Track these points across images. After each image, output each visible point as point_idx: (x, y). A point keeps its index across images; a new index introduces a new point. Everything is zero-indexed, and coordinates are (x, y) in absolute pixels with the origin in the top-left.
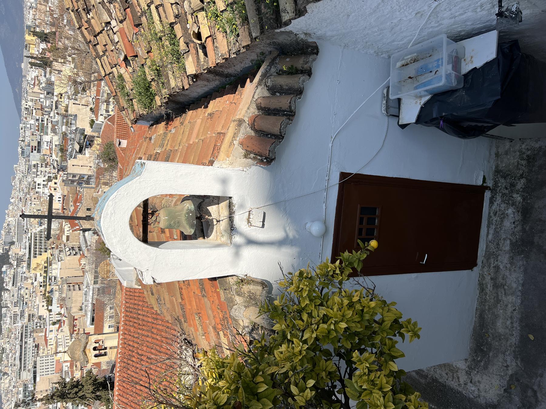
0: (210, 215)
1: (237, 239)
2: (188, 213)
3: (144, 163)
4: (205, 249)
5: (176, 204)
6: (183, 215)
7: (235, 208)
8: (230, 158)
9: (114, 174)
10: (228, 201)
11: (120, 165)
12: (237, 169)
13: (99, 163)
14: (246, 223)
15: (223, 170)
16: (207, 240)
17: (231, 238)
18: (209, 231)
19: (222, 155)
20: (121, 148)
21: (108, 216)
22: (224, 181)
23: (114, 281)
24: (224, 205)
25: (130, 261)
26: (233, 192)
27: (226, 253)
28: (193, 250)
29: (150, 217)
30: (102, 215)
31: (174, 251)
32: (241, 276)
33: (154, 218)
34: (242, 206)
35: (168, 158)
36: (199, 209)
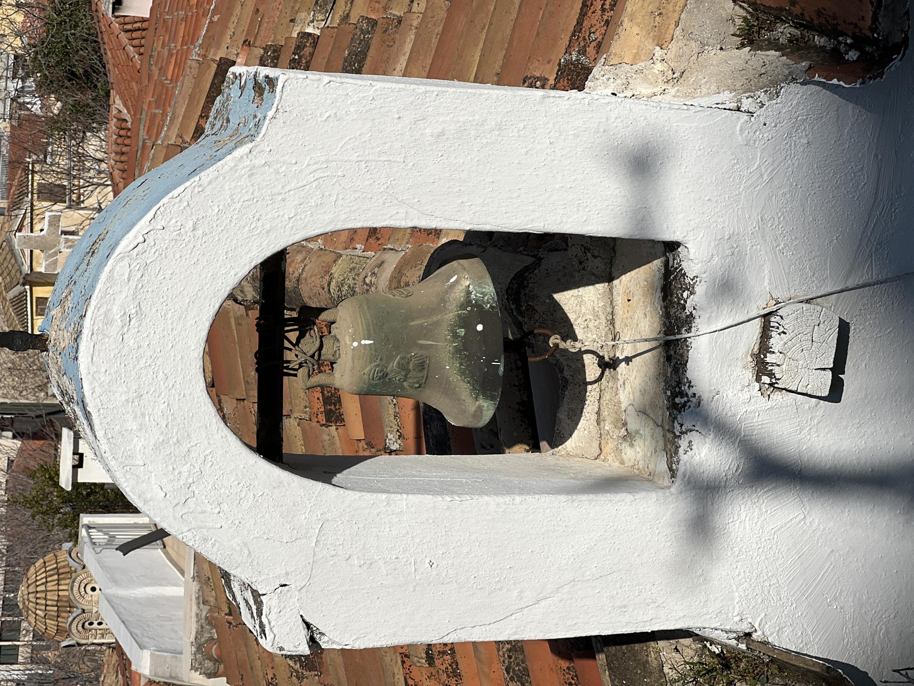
0: (569, 333)
1: (704, 454)
2: (466, 322)
3: (271, 82)
4: (546, 500)
5: (397, 282)
6: (444, 332)
7: (695, 300)
8: (674, 47)
9: (93, 146)
10: (657, 263)
11: (117, 103)
12: (705, 101)
13: (21, 92)
14: (749, 375)
15: (638, 108)
16: (547, 456)
17: (670, 448)
18: (562, 415)
19: (631, 34)
20: (125, 21)
21: (114, 330)
22: (642, 164)
23: (91, 654)
24: (635, 284)
25: (205, 540)
26: (697, 216)
27: (649, 519)
28: (491, 503)
29: (293, 336)
30: (87, 322)
31: (402, 501)
32: (722, 637)
33: (309, 344)
34: (727, 288)
35: (357, 56)
36: (517, 301)
